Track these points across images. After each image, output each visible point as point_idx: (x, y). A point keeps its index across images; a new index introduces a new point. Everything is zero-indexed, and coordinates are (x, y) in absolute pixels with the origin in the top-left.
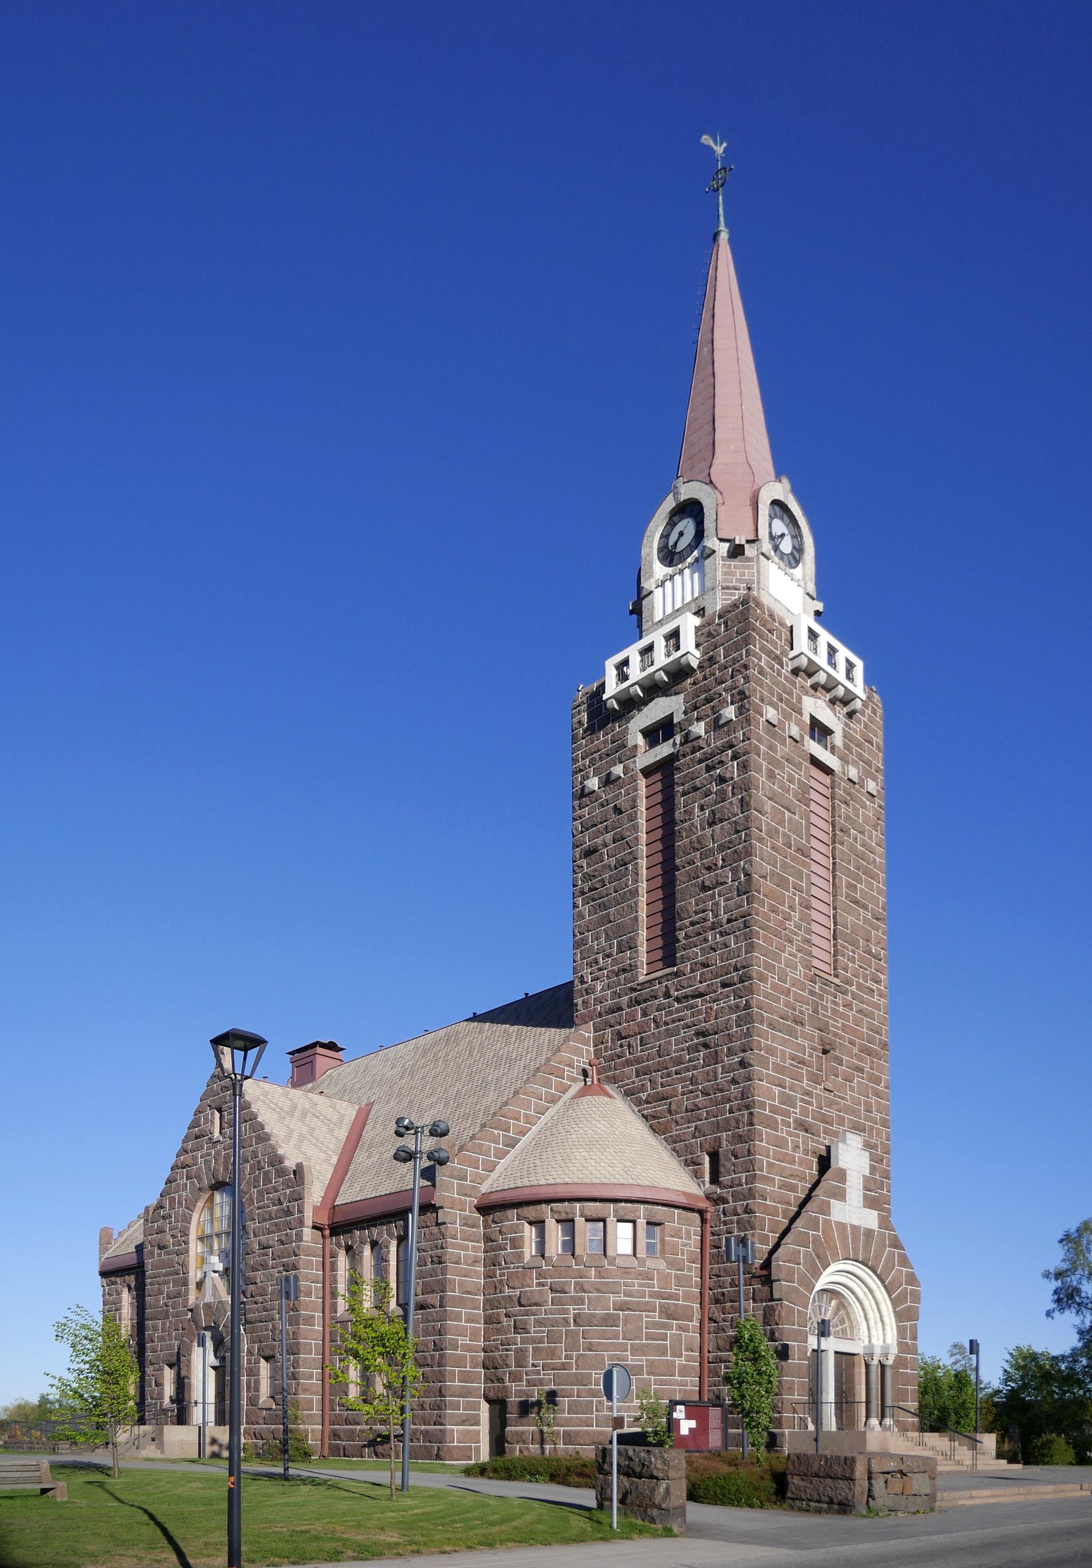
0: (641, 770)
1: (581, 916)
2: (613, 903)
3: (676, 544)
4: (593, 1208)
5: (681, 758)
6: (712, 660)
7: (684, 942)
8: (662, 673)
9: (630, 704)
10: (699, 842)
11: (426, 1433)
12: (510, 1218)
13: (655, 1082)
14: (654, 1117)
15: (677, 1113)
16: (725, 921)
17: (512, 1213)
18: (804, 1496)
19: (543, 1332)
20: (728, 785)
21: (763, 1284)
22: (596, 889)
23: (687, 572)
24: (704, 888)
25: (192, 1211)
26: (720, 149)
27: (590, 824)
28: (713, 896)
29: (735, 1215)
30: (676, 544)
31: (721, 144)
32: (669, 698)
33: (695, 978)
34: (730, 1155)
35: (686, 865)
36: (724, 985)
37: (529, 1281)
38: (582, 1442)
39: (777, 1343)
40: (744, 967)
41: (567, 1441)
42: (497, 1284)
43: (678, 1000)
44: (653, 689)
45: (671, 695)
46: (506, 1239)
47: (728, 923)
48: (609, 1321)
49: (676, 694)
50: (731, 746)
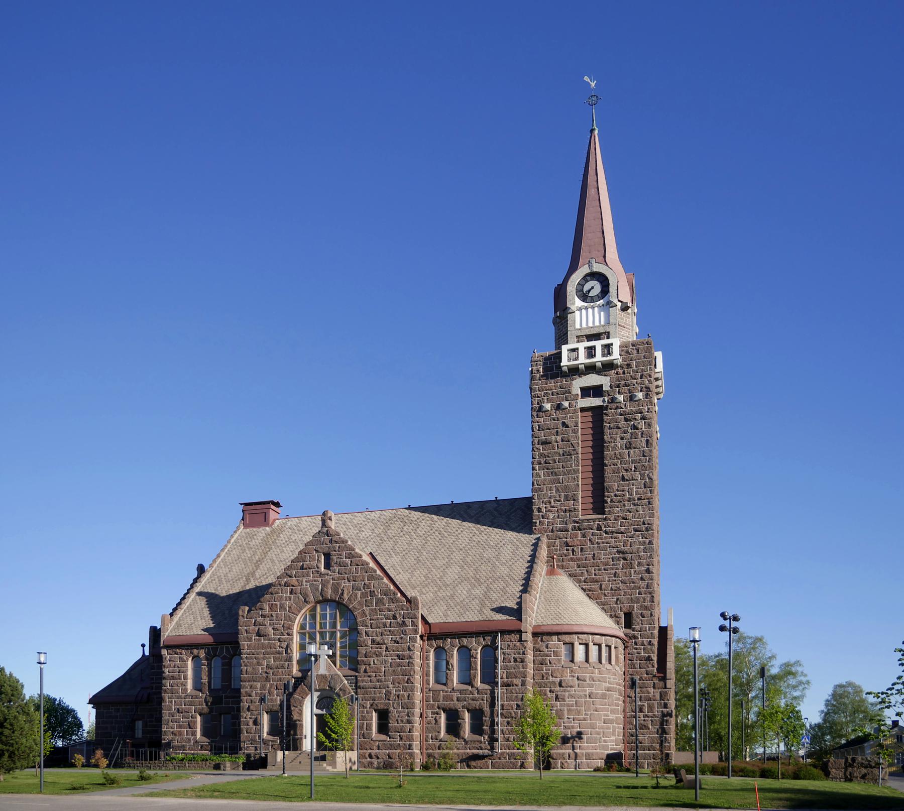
0: (580, 408)
1: (538, 475)
2: (562, 474)
3: (589, 291)
4: (597, 638)
5: (609, 409)
6: (629, 366)
7: (610, 504)
8: (600, 363)
9: (575, 371)
10: (620, 455)
11: (513, 754)
12: (554, 640)
13: (590, 572)
14: (590, 591)
15: (605, 590)
16: (636, 499)
17: (555, 638)
18: (838, 777)
19: (573, 701)
20: (639, 432)
21: (660, 680)
22: (550, 463)
23: (596, 309)
24: (623, 479)
25: (297, 616)
26: (593, 84)
27: (546, 428)
28: (629, 485)
29: (642, 645)
30: (589, 291)
31: (594, 82)
32: (600, 376)
33: (617, 524)
34: (639, 616)
35: (612, 465)
36: (636, 531)
37: (565, 674)
38: (595, 758)
39: (668, 709)
40: (649, 524)
41: (587, 758)
42: (544, 675)
43: (606, 532)
44: (591, 369)
45: (602, 375)
46: (551, 651)
47: (638, 500)
48: (603, 696)
49: (605, 375)
50: (641, 413)
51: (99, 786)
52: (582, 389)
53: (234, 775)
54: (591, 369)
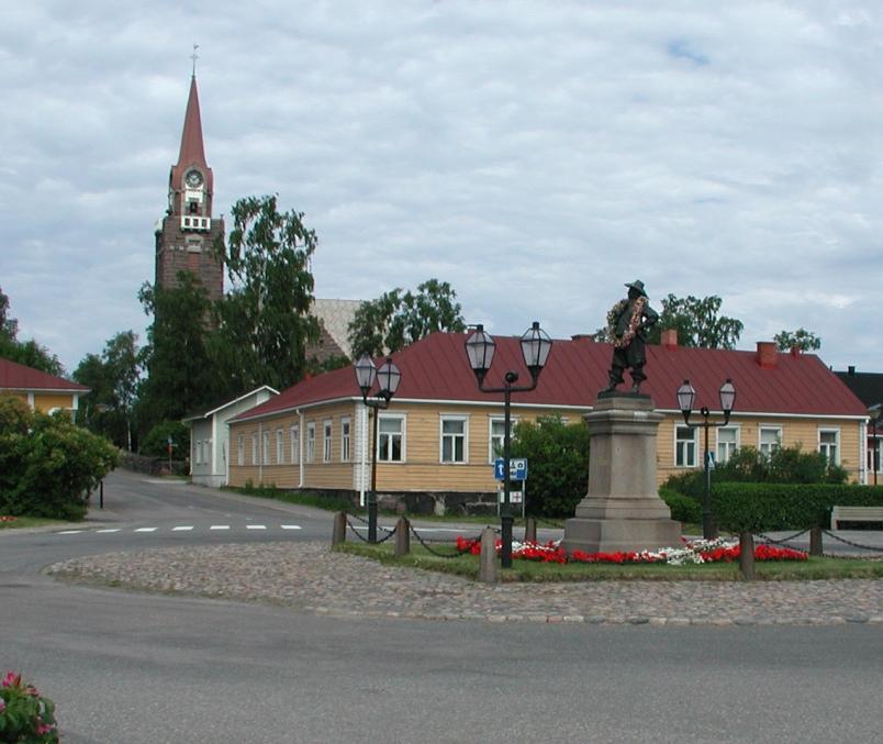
44: (196, 231)
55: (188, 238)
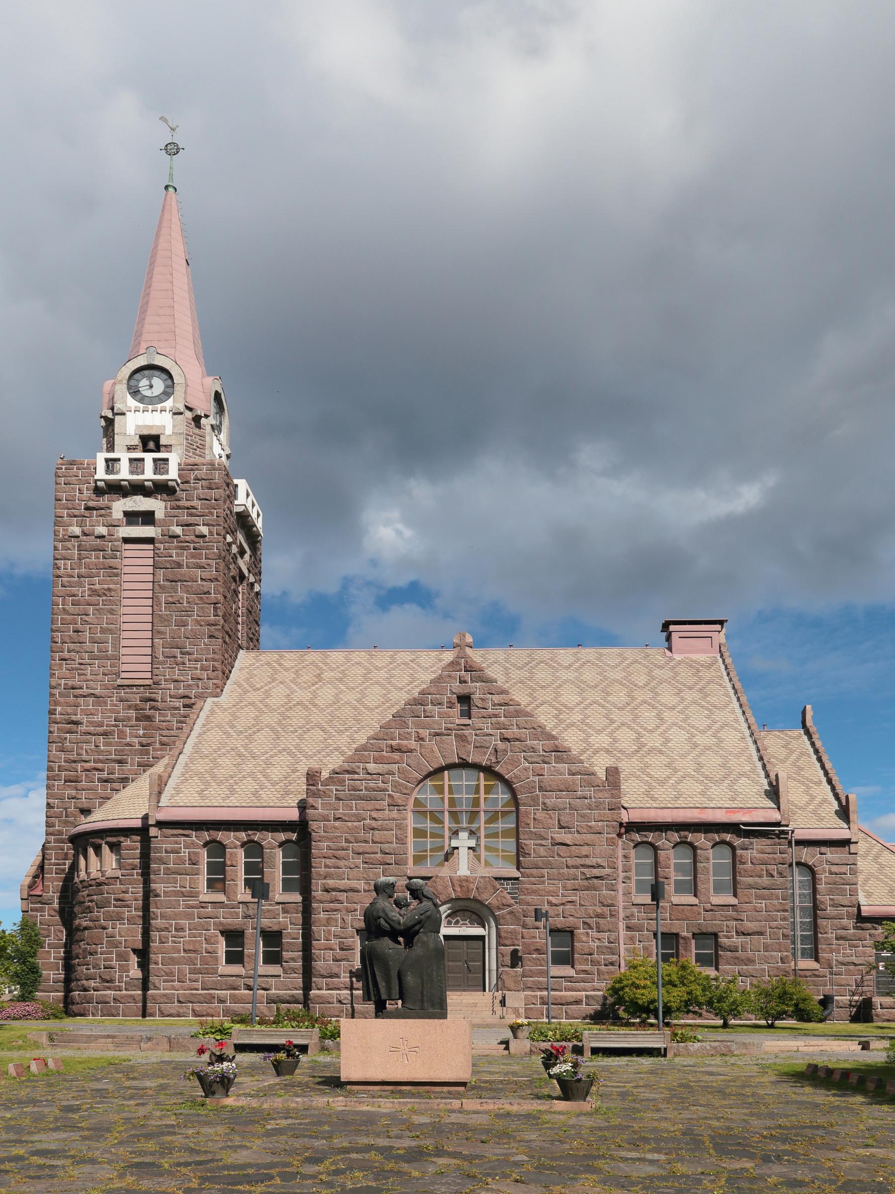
44: (138, 489)
51: (748, 1029)
52: (127, 514)
53: (865, 1037)
54: (138, 489)
55: (120, 506)
